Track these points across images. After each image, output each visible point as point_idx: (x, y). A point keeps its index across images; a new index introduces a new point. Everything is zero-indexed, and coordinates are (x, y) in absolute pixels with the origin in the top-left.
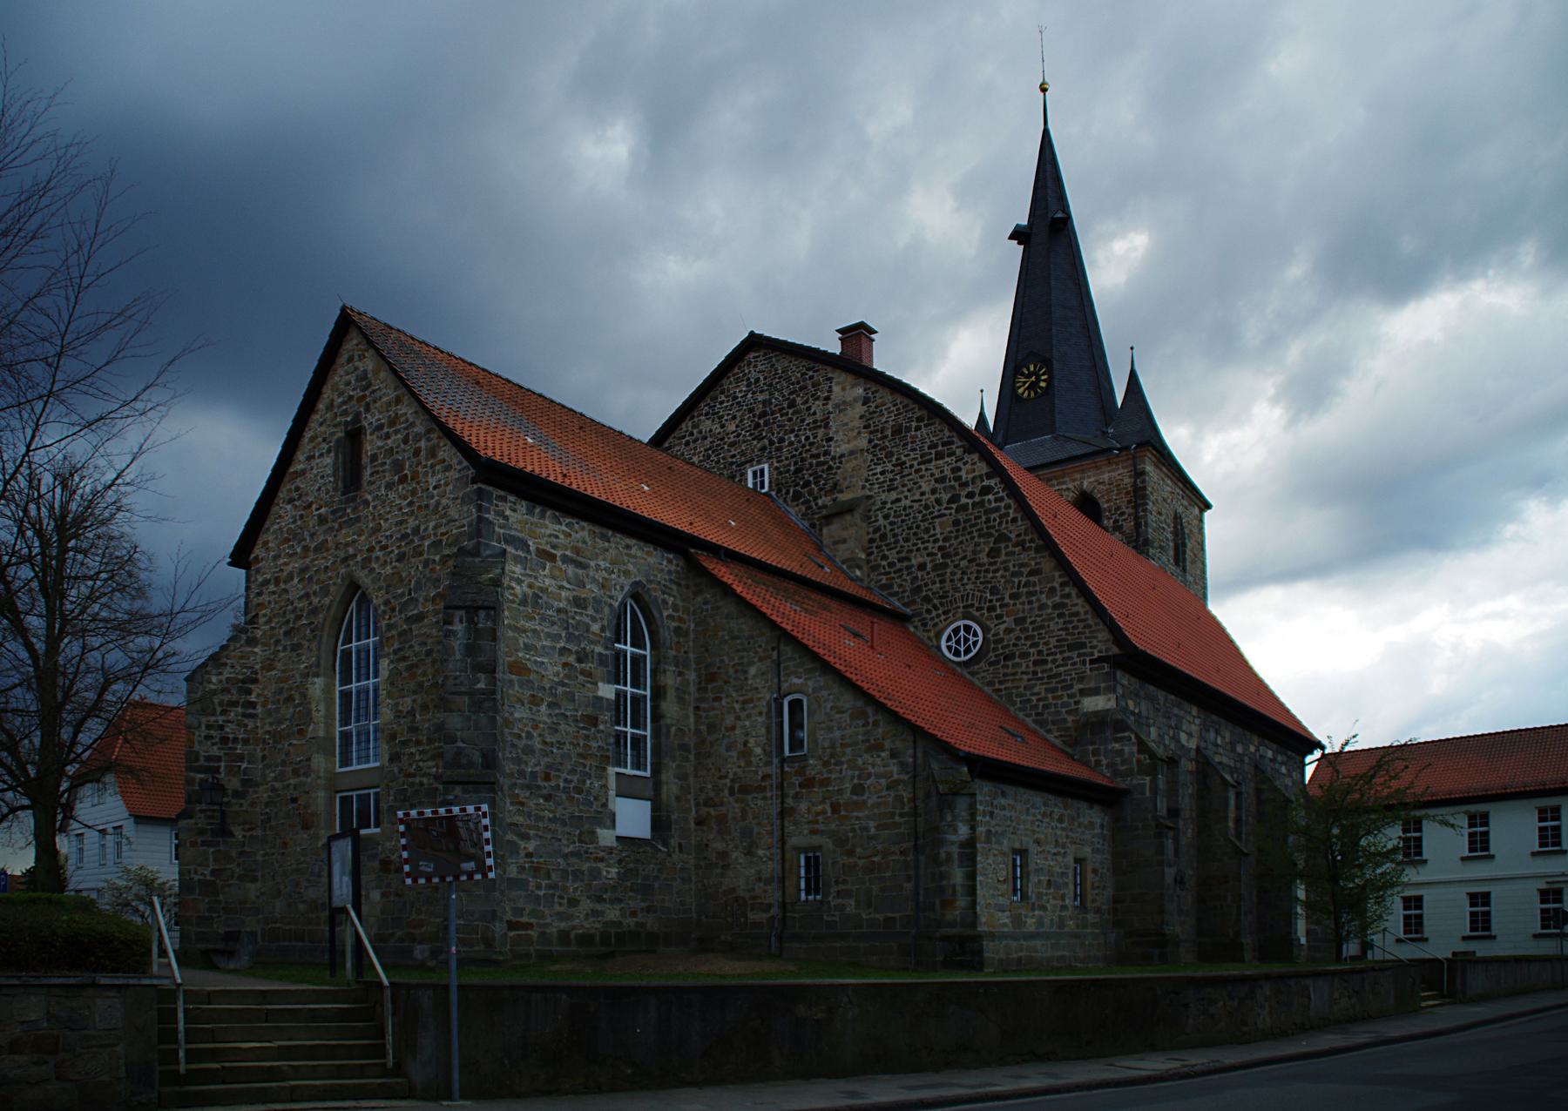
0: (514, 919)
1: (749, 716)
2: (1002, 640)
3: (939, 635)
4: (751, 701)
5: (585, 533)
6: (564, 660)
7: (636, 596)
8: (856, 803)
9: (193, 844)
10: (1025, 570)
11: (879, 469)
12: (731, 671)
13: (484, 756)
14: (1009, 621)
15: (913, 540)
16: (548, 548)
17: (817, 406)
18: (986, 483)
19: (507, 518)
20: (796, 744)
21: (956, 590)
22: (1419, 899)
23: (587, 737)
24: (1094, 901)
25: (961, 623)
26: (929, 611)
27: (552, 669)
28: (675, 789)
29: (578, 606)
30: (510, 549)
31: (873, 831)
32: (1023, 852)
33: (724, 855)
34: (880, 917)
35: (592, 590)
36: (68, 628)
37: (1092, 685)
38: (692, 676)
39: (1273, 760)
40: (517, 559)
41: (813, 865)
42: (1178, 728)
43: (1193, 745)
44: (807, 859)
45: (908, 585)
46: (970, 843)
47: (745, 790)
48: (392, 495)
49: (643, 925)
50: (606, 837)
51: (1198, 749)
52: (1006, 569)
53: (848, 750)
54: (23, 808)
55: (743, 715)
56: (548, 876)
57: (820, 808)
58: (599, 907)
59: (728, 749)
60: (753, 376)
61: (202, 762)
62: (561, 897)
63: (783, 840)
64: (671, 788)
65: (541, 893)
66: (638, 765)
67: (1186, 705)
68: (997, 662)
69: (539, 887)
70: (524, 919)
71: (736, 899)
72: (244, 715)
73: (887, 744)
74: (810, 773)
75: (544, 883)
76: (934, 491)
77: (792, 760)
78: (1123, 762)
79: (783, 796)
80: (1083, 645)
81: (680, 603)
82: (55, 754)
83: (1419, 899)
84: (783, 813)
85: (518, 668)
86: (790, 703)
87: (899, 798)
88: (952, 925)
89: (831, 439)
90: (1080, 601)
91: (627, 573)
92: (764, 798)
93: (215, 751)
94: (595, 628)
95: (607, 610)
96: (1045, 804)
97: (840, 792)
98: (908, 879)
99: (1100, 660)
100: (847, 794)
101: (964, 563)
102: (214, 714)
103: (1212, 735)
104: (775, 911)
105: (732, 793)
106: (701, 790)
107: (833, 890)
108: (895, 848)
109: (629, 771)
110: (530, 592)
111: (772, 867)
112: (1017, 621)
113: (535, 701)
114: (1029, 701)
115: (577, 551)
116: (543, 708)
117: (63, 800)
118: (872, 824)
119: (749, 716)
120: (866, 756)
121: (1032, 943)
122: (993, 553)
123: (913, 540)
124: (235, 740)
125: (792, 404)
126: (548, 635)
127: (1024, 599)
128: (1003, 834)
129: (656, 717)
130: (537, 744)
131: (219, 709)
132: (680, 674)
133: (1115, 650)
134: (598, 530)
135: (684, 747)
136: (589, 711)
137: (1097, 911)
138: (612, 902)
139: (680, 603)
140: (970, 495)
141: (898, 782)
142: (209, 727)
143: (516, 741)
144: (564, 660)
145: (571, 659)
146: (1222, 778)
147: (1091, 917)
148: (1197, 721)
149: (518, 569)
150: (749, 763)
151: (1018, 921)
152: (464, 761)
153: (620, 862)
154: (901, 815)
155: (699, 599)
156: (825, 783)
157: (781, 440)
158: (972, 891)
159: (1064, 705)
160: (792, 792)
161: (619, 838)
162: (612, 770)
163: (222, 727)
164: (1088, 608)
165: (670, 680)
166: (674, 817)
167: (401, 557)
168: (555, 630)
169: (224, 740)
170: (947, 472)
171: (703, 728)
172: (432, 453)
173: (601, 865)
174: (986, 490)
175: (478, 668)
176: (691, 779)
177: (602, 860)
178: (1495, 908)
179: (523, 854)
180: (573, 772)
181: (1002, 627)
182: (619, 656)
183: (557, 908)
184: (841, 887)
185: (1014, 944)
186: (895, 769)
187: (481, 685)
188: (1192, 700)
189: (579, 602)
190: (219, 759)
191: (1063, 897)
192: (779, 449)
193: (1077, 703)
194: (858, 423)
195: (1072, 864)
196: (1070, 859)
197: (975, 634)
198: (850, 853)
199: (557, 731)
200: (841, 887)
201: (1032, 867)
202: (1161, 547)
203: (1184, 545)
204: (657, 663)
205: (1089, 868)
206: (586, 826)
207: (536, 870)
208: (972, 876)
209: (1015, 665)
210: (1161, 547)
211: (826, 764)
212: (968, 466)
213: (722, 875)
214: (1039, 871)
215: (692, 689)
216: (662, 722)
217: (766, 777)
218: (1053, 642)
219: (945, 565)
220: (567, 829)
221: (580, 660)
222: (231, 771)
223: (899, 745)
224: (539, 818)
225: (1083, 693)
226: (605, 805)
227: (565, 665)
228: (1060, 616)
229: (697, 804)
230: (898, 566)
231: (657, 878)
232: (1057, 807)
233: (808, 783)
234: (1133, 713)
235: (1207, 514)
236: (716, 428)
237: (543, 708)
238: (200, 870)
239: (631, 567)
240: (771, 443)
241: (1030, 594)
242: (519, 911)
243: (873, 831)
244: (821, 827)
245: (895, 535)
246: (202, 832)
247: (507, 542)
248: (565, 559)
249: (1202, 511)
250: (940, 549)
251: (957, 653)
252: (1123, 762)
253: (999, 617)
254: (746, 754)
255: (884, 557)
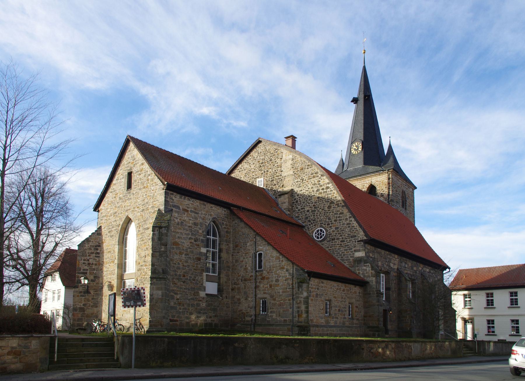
1: (247, 258)
2: (331, 234)
3: (313, 232)
4: (248, 253)
5: (198, 204)
6: (190, 241)
7: (214, 222)
8: (276, 285)
9: (78, 296)
10: (339, 213)
11: (296, 180)
12: (242, 244)
13: (163, 270)
14: (334, 228)
16: (186, 208)
17: (278, 161)
18: (327, 185)
19: (173, 200)
20: (260, 267)
22: (493, 321)
23: (197, 264)
24: (356, 316)
25: (319, 229)
26: (310, 225)
27: (186, 244)
28: (225, 280)
29: (195, 225)
30: (174, 209)
31: (281, 293)
32: (330, 301)
33: (239, 299)
35: (200, 220)
36: (44, 227)
37: (358, 249)
38: (231, 245)
39: (429, 272)
40: (176, 212)
41: (264, 303)
43: (396, 267)
44: (263, 301)
45: (304, 217)
46: (307, 298)
47: (245, 280)
48: (140, 192)
49: (214, 321)
50: (202, 294)
51: (398, 269)
52: (333, 212)
53: (274, 269)
54: (27, 285)
55: (245, 257)
56: (183, 305)
57: (266, 286)
58: (199, 315)
59: (241, 267)
60: (259, 151)
62: (187, 312)
63: (256, 296)
64: (224, 279)
65: (181, 311)
66: (214, 272)
67: (393, 255)
68: (330, 241)
69: (180, 309)
70: (175, 319)
72: (96, 257)
73: (285, 267)
74: (264, 275)
75: (182, 308)
76: (312, 188)
77: (259, 271)
78: (367, 273)
80: (355, 236)
82: (37, 268)
83: (493, 321)
84: (256, 287)
86: (259, 254)
87: (288, 284)
88: (301, 322)
89: (282, 171)
90: (355, 222)
91: (211, 215)
92: (251, 283)
93: (86, 267)
94: (201, 231)
95: (204, 226)
96: (338, 286)
97: (272, 281)
98: (291, 308)
101: (320, 210)
102: (86, 256)
103: (403, 264)
104: (253, 317)
105: (242, 281)
106: (233, 280)
107: (270, 311)
108: (287, 298)
109: (211, 274)
110: (180, 221)
111: (252, 304)
112: (336, 228)
113: (181, 253)
114: (339, 253)
116: (183, 256)
117: (40, 281)
118: (281, 291)
119: (247, 258)
120: (280, 271)
121: (332, 329)
122: (329, 207)
124: (93, 264)
125: (271, 160)
126: (185, 234)
127: (338, 221)
128: (322, 295)
130: (181, 266)
131: (88, 255)
132: (227, 245)
133: (365, 238)
134: (202, 202)
135: (228, 267)
136: (198, 256)
137: (358, 319)
138: (203, 314)
140: (323, 189)
141: (288, 279)
142: (84, 260)
143: (174, 265)
144: (190, 241)
145: (193, 241)
146: (405, 278)
147: (355, 321)
148: (397, 260)
149: (176, 215)
150: (247, 272)
152: (157, 271)
153: (207, 301)
154: (289, 289)
155: (234, 222)
156: (268, 278)
157: (267, 171)
158: (307, 312)
160: (258, 281)
161: (206, 294)
162: (205, 274)
163: (88, 260)
164: (357, 224)
165: (224, 247)
167: (143, 210)
168: (188, 232)
169: (89, 264)
170: (316, 182)
172: (152, 180)
173: (200, 302)
174: (328, 188)
175: (162, 244)
177: (201, 301)
179: (175, 299)
180: (192, 274)
181: (331, 230)
183: (186, 315)
185: (325, 329)
186: (287, 275)
187: (163, 249)
188: (395, 253)
190: (87, 270)
191: (344, 315)
192: (267, 174)
193: (353, 254)
194: (290, 166)
195: (348, 305)
196: (347, 303)
197: (323, 232)
198: (275, 300)
199: (187, 262)
202: (397, 202)
203: (406, 201)
204: (220, 241)
205: (354, 306)
206: (196, 291)
208: (307, 308)
209: (335, 242)
210: (397, 202)
211: (268, 273)
212: (322, 180)
215: (231, 249)
216: (222, 259)
217: (251, 276)
218: (347, 235)
219: (315, 211)
221: (195, 241)
222: (90, 273)
223: (289, 267)
225: (355, 251)
226: (202, 284)
227: (191, 242)
229: (232, 284)
230: (301, 211)
231: (218, 306)
232: (342, 286)
233: (263, 278)
234: (372, 257)
235: (415, 191)
236: (248, 166)
237: (183, 256)
238: (79, 304)
239: (212, 213)
240: (264, 172)
241: (340, 220)
242: (174, 316)
243: (281, 293)
244: (267, 292)
245: (300, 201)
246: (81, 292)
247: (173, 207)
248: (191, 211)
249: (413, 190)
250: (314, 205)
251: (318, 238)
252: (367, 273)
254: (246, 269)
255: (297, 208)
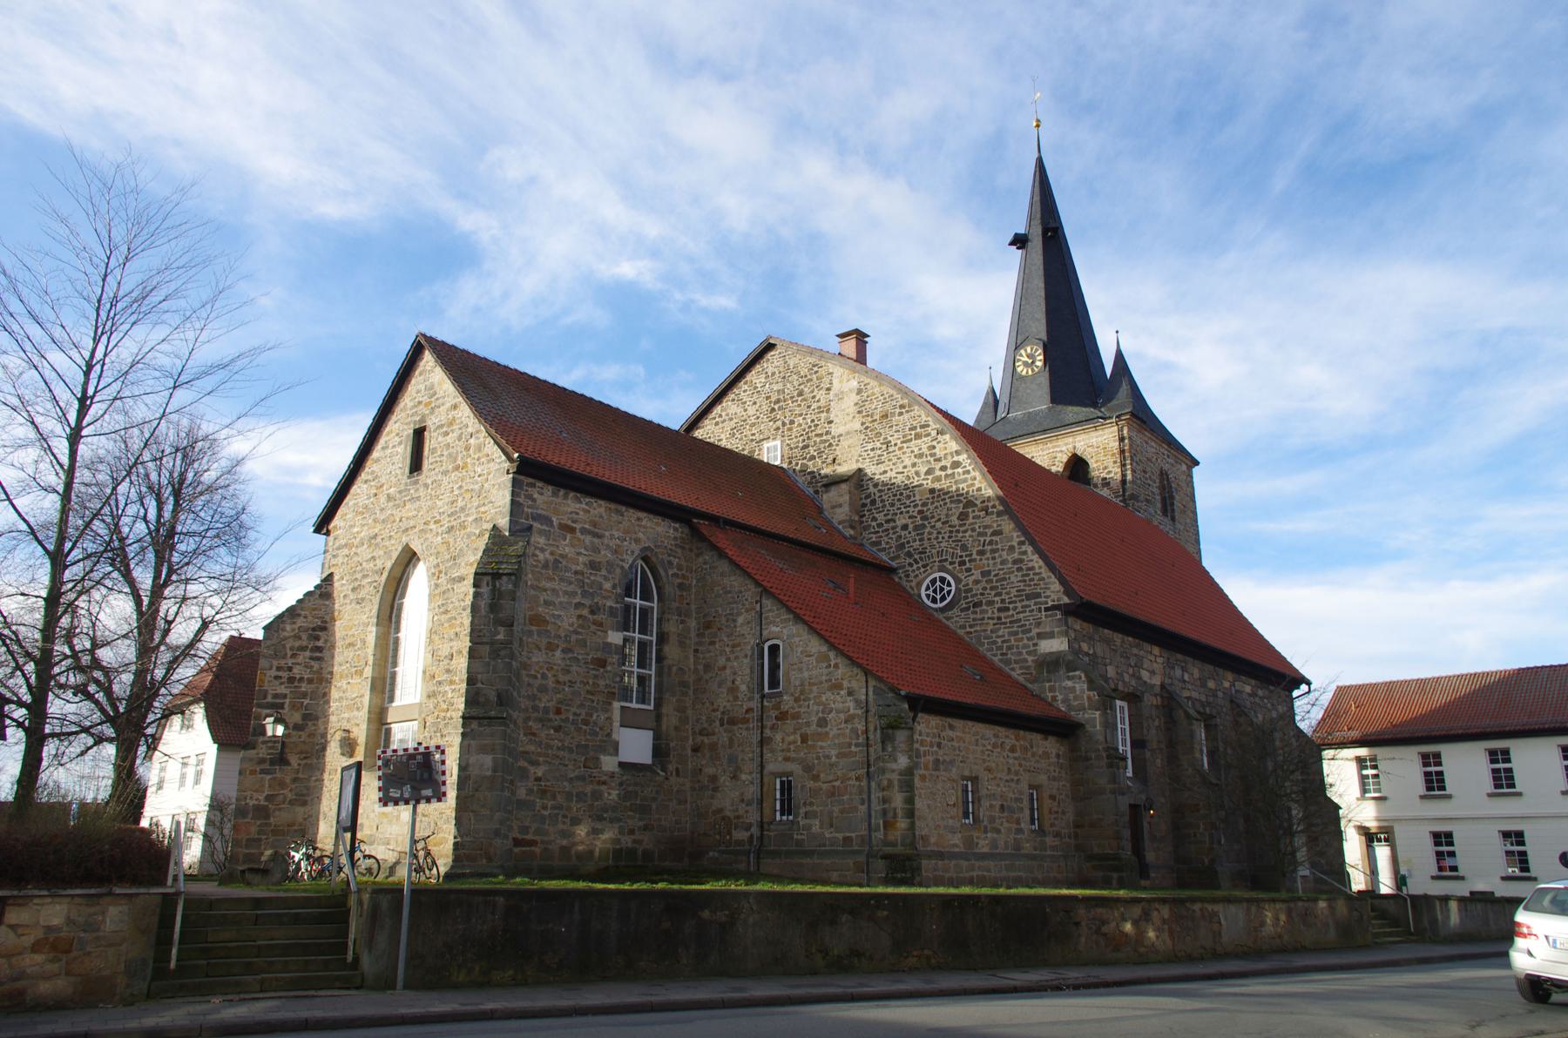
0: (520, 836)
3: (919, 585)
6: (578, 612)
7: (645, 559)
9: (253, 772)
10: (989, 531)
11: (870, 446)
12: (724, 620)
14: (977, 574)
15: (898, 504)
17: (821, 395)
19: (534, 500)
20: (774, 683)
21: (933, 547)
22: (1449, 835)
24: (1052, 825)
25: (937, 575)
26: (910, 565)
28: (674, 721)
30: (536, 525)
32: (975, 780)
33: (714, 778)
34: (840, 836)
35: (606, 555)
36: (174, 577)
37: (1048, 630)
38: (693, 624)
39: (1253, 695)
40: (541, 532)
41: (787, 788)
42: (1139, 666)
43: (1157, 681)
44: (782, 783)
45: (893, 543)
46: (909, 772)
47: (732, 722)
50: (609, 763)
51: (1163, 686)
52: (973, 530)
53: (815, 688)
54: (111, 740)
56: (554, 797)
57: (792, 738)
59: (720, 685)
61: (269, 699)
62: (565, 816)
63: (762, 766)
64: (671, 718)
65: (546, 813)
67: (1147, 646)
68: (967, 609)
69: (545, 808)
71: (723, 818)
72: (311, 658)
73: (846, 684)
74: (784, 707)
75: (550, 804)
76: (914, 465)
77: (771, 696)
78: (1076, 698)
79: (762, 727)
80: (1038, 595)
81: (683, 563)
82: (145, 690)
83: (1449, 835)
84: (762, 743)
85: (537, 620)
90: (1036, 557)
91: (637, 541)
93: (282, 690)
95: (618, 571)
96: (996, 736)
97: (808, 724)
99: (1054, 608)
100: (814, 727)
101: (939, 525)
102: (284, 657)
103: (1178, 672)
104: (755, 830)
107: (802, 811)
109: (634, 705)
110: (551, 558)
111: (752, 791)
112: (984, 574)
113: (551, 647)
114: (995, 643)
115: (594, 524)
117: (149, 731)
121: (985, 863)
123: (898, 504)
126: (566, 593)
128: (952, 762)
129: (660, 659)
130: (550, 683)
131: (289, 653)
132: (682, 622)
133: (1066, 600)
134: (613, 506)
135: (684, 684)
136: (599, 655)
138: (611, 821)
139: (683, 563)
144: (578, 612)
145: (585, 612)
146: (1186, 713)
147: (1049, 840)
148: (1160, 660)
149: (542, 540)
150: (736, 699)
151: (969, 843)
152: (482, 699)
154: (857, 745)
156: (796, 716)
157: (792, 422)
158: (911, 814)
159: (1025, 646)
160: (769, 724)
161: (621, 764)
162: (617, 705)
163: (290, 669)
166: (672, 745)
167: (451, 529)
168: (570, 588)
169: (291, 680)
170: (925, 450)
171: (701, 667)
172: (479, 448)
173: (603, 788)
174: (956, 465)
176: (689, 712)
177: (604, 783)
178: (1529, 848)
180: (582, 706)
182: (628, 609)
183: (561, 826)
184: (808, 808)
185: (964, 863)
186: (851, 705)
187: (500, 637)
189: (593, 565)
190: (285, 696)
196: (1024, 786)
197: (949, 585)
198: (816, 778)
199: (569, 672)
200: (808, 808)
201: (983, 792)
203: (1172, 498)
204: (662, 613)
205: (1045, 795)
207: (543, 792)
208: (910, 801)
213: (712, 797)
214: (992, 796)
215: (693, 634)
219: (924, 526)
220: (574, 756)
221: (592, 612)
222: (293, 707)
223: (854, 685)
224: (549, 747)
225: (1040, 636)
226: (609, 735)
227: (580, 616)
228: (1019, 569)
231: (654, 799)
232: (1007, 736)
233: (782, 716)
234: (1087, 654)
235: (1195, 470)
236: (739, 410)
237: (558, 653)
239: (641, 535)
242: (525, 830)
246: (262, 761)
247: (534, 519)
248: (583, 531)
249: (1190, 468)
250: (920, 512)
252: (1076, 698)
253: (969, 570)
254: (733, 690)
255: (874, 519)
